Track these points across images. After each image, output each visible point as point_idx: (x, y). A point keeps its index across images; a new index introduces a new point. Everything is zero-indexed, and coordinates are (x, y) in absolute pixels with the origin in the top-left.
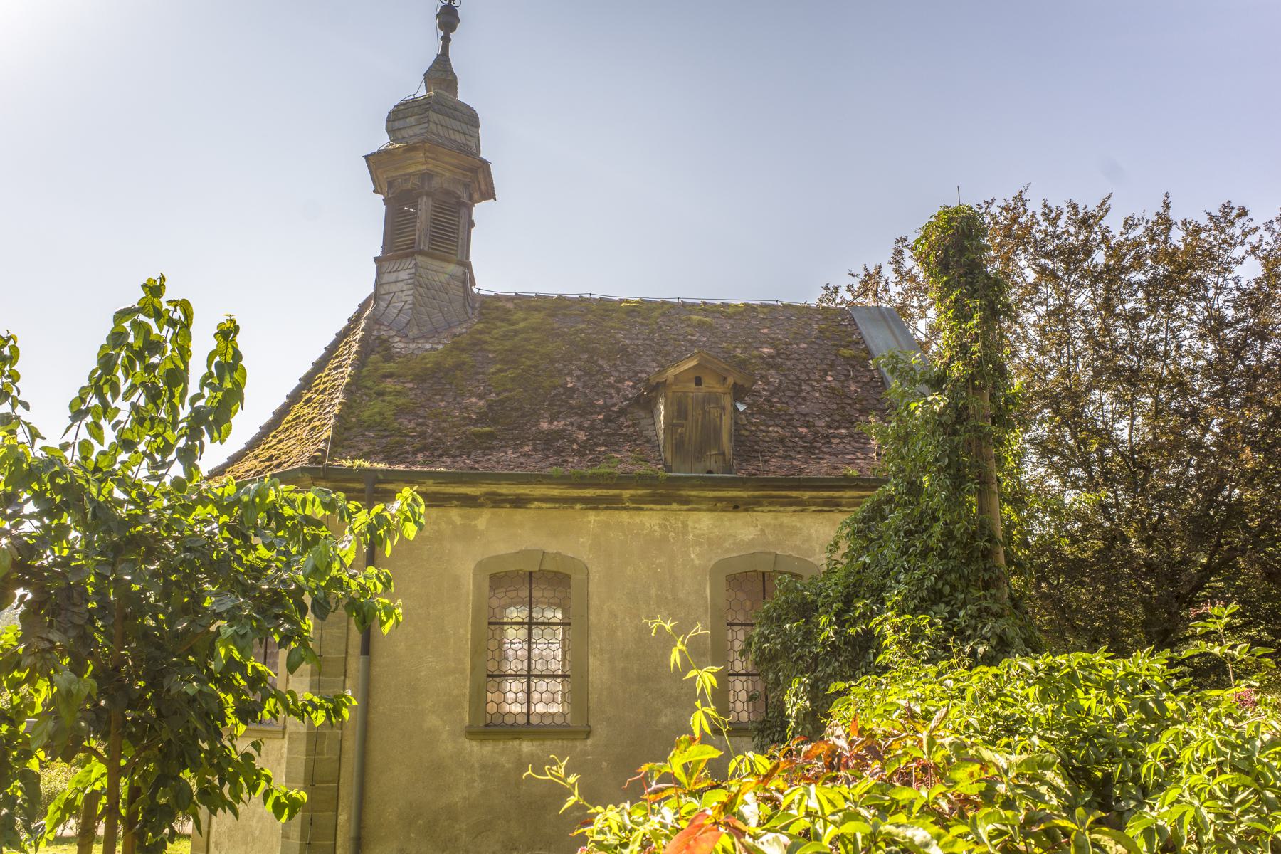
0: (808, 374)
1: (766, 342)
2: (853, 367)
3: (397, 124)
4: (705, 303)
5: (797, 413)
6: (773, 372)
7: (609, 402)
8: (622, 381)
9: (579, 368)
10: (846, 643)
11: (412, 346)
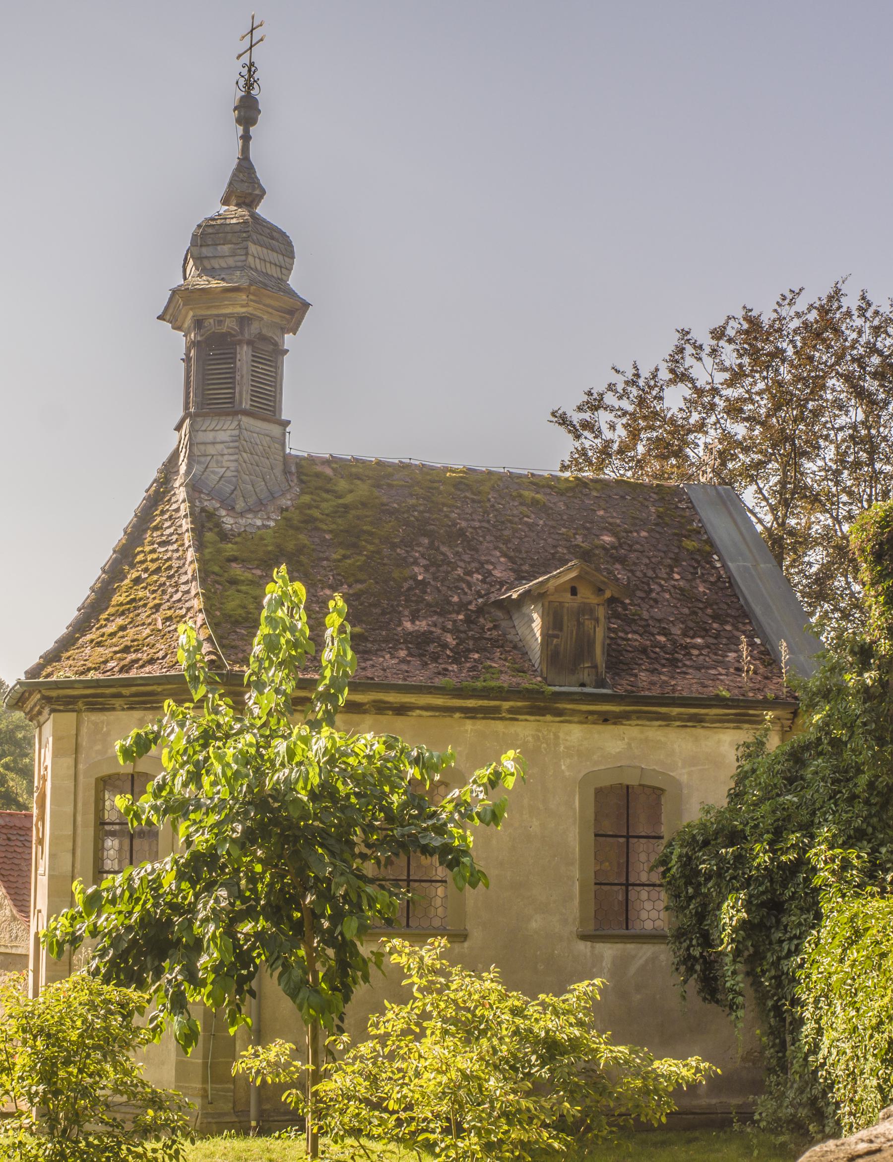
0: (654, 570)
1: (605, 528)
2: (698, 562)
3: (205, 251)
4: (533, 475)
5: (652, 617)
6: (618, 566)
7: (466, 599)
8: (469, 573)
9: (423, 556)
10: (778, 867)
11: (242, 521)
